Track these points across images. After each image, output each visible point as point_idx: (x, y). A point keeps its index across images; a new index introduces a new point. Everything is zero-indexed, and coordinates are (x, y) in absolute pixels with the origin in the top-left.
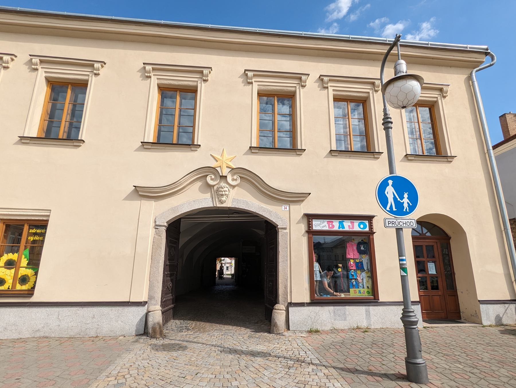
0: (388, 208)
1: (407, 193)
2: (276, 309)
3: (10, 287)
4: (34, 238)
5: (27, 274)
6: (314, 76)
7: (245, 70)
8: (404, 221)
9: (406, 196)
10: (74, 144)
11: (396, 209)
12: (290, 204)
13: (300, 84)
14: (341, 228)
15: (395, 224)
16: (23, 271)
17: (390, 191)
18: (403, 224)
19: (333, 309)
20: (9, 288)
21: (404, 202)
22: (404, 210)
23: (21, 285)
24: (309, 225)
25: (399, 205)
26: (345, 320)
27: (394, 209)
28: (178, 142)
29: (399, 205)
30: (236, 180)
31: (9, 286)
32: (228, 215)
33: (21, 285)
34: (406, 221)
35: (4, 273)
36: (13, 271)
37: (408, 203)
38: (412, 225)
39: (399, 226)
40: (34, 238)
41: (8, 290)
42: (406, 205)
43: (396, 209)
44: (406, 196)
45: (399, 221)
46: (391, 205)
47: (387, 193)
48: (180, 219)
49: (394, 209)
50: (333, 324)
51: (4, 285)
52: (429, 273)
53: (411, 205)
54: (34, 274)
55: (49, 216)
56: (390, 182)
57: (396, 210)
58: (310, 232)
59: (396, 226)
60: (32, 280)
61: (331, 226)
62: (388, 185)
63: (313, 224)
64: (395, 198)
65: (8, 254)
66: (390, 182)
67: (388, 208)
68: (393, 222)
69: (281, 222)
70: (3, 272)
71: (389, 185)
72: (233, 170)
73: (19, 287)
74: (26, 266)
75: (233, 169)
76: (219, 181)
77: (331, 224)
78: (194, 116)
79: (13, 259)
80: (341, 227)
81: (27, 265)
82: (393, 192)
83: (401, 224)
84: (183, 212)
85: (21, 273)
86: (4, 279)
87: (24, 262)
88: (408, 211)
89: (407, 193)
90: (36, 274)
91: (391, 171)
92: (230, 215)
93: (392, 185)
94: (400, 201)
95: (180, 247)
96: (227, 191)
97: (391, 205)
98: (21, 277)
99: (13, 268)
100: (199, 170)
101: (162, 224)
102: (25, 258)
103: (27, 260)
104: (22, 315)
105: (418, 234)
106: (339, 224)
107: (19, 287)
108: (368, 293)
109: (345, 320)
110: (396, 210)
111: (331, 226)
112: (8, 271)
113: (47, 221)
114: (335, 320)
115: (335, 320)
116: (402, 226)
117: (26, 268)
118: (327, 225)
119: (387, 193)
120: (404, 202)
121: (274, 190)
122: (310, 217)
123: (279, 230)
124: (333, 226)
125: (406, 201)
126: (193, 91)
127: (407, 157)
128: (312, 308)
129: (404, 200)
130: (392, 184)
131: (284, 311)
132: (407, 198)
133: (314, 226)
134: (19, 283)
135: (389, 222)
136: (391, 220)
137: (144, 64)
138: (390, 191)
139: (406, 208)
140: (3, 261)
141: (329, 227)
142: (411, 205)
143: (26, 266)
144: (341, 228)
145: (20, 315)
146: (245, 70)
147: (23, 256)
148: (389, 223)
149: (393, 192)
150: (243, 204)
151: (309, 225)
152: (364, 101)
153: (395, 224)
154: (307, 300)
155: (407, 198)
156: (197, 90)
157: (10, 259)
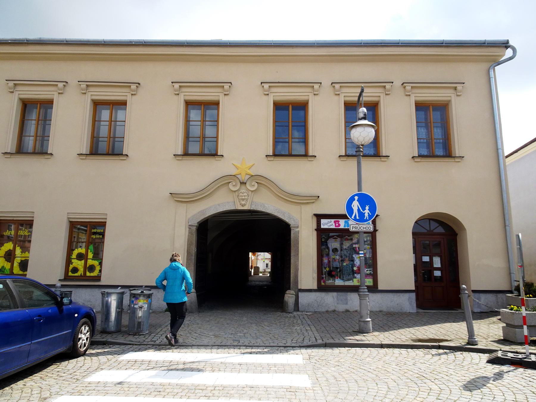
0: (353, 217)
1: (369, 206)
2: (287, 294)
3: (82, 274)
4: (96, 236)
5: (93, 264)
6: (326, 83)
7: (261, 83)
8: (364, 226)
9: (367, 208)
10: (120, 159)
11: (354, 218)
12: (301, 206)
13: (313, 92)
14: (346, 227)
15: (357, 228)
16: (90, 262)
17: (356, 205)
18: (363, 228)
19: (336, 295)
20: (81, 275)
21: (365, 213)
22: (365, 219)
23: (90, 273)
24: (319, 224)
25: (361, 215)
26: (347, 304)
27: (358, 218)
28: (206, 141)
29: (361, 215)
30: (254, 185)
31: (81, 273)
32: (250, 214)
33: (90, 273)
34: (366, 226)
35: (77, 264)
36: (83, 262)
37: (368, 213)
38: (367, 229)
39: (360, 230)
40: (96, 236)
41: (81, 276)
42: (366, 215)
43: (354, 218)
44: (367, 208)
45: (360, 226)
46: (356, 215)
47: (353, 206)
48: (208, 219)
49: (358, 218)
50: (336, 307)
51: (78, 273)
52: (434, 266)
53: (370, 214)
54: (99, 264)
55: (106, 219)
56: (356, 198)
57: (359, 218)
58: (320, 231)
59: (358, 230)
60: (98, 268)
61: (337, 225)
62: (354, 200)
63: (321, 223)
64: (359, 210)
65: (19, 247)
66: (356, 198)
67: (353, 217)
68: (356, 227)
69: (293, 222)
70: (76, 262)
71: (355, 200)
72: (253, 177)
73: (88, 274)
74: (92, 258)
75: (252, 176)
76: (240, 187)
77: (337, 223)
78: (216, 141)
79: (82, 253)
80: (346, 225)
81: (92, 257)
82: (358, 206)
83: (362, 228)
84: (210, 215)
85: (88, 263)
86: (77, 268)
87: (90, 255)
88: (368, 219)
89: (369, 206)
90: (101, 264)
91: (360, 188)
92: (253, 214)
93: (357, 200)
94: (363, 212)
95: (208, 244)
96: (246, 196)
97: (356, 215)
98: (89, 266)
99: (83, 260)
100: (221, 179)
101: (194, 225)
102: (90, 252)
103: (92, 254)
104: (94, 295)
105: (426, 231)
106: (344, 223)
107: (88, 274)
108: (369, 282)
109: (347, 304)
110: (359, 218)
111: (337, 225)
112: (79, 262)
113: (106, 222)
114: (338, 304)
115: (338, 304)
116: (363, 230)
117: (92, 259)
118: (334, 224)
119: (353, 206)
120: (365, 213)
121: (287, 194)
122: (319, 217)
123: (292, 229)
124: (339, 225)
125: (367, 212)
126: (217, 104)
127: (414, 159)
128: (318, 294)
129: (365, 211)
130: (357, 199)
131: (294, 296)
132: (368, 209)
133: (322, 225)
134: (88, 271)
135: (353, 227)
136: (354, 226)
137: (172, 82)
138: (356, 205)
139: (367, 217)
140: (75, 254)
141: (336, 226)
142: (370, 214)
143: (92, 258)
144: (346, 227)
145: (93, 294)
146: (261, 83)
147: (89, 251)
148: (353, 228)
149: (358, 206)
150: (260, 207)
151: (319, 224)
152: (376, 104)
153: (357, 228)
154: (315, 287)
155: (368, 209)
156: (219, 103)
157: (414, 254)
